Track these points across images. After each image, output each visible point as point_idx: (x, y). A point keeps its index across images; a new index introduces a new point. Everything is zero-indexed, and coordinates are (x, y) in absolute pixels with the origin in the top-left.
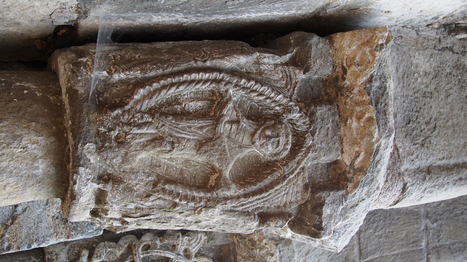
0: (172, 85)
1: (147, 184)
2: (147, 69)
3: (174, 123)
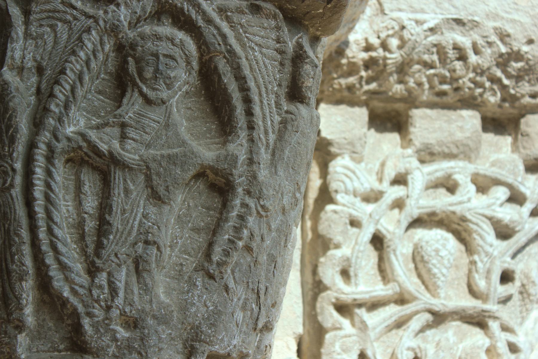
0: (50, 231)
1: (206, 289)
2: (20, 270)
3: (115, 238)
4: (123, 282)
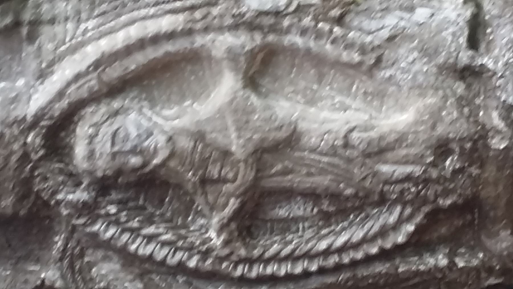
1: (393, 64)
4: (394, 167)
